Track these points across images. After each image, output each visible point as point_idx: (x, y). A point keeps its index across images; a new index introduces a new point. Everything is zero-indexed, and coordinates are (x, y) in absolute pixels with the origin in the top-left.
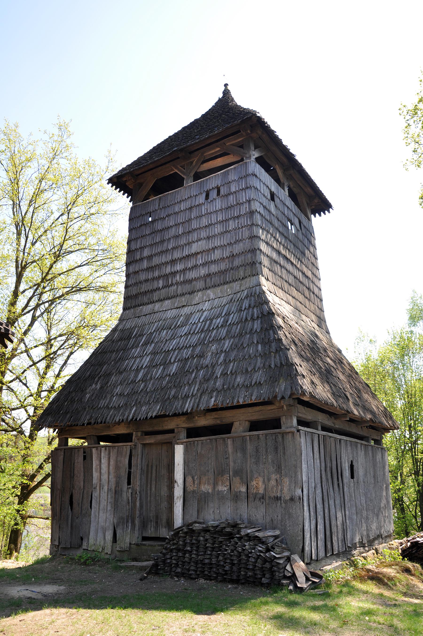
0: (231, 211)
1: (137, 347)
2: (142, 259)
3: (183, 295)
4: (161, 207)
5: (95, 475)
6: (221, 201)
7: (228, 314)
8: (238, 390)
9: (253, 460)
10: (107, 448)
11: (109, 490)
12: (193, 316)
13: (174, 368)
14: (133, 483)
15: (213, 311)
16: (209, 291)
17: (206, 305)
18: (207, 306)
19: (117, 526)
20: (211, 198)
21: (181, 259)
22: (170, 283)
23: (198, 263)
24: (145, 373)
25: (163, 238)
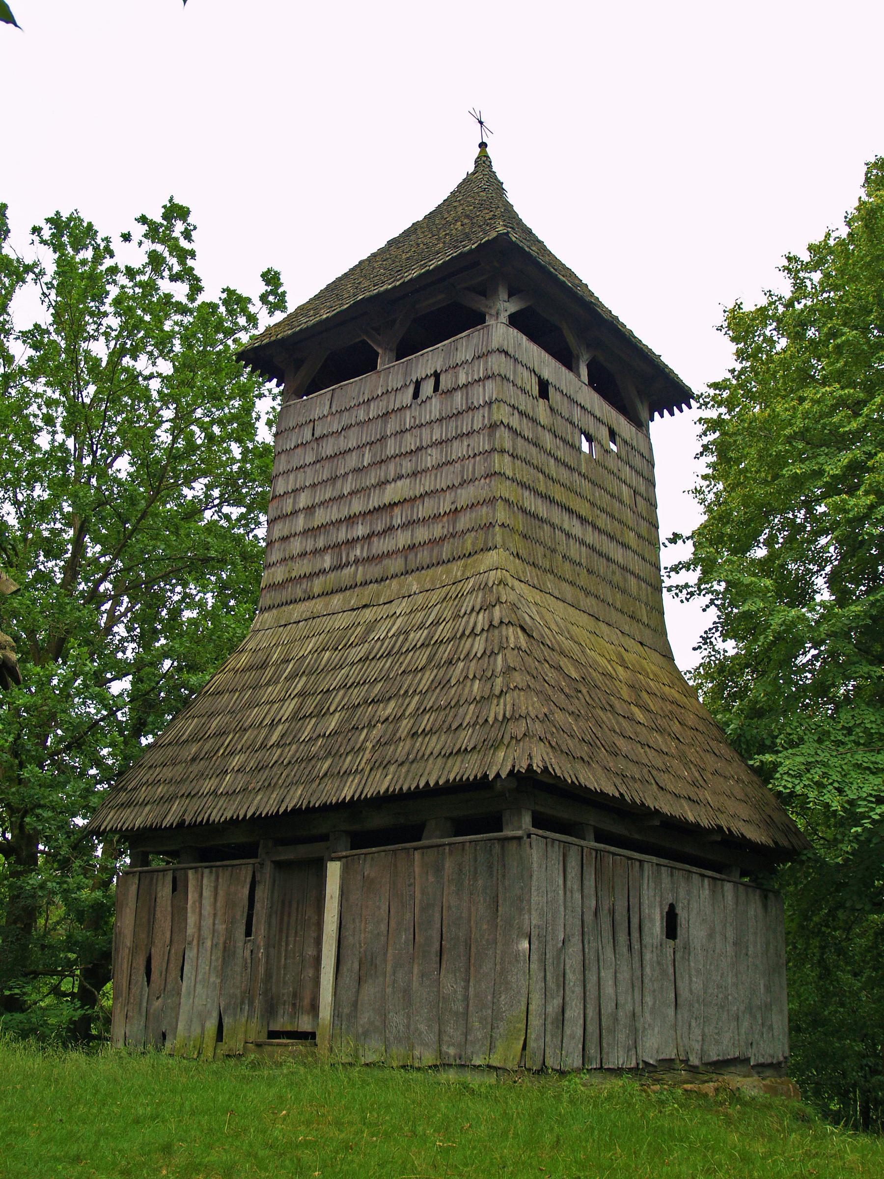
0: (456, 422)
1: (277, 682)
2: (294, 513)
3: (365, 584)
4: (334, 410)
5: (191, 919)
6: (441, 403)
7: (436, 623)
8: (430, 762)
9: (453, 888)
10: (214, 869)
11: (214, 946)
12: (379, 625)
13: (333, 723)
14: (256, 932)
15: (413, 615)
16: (410, 578)
17: (404, 604)
18: (402, 607)
19: (225, 1013)
20: (423, 396)
21: (364, 515)
22: (344, 560)
23: (394, 523)
24: (283, 732)
25: (336, 472)
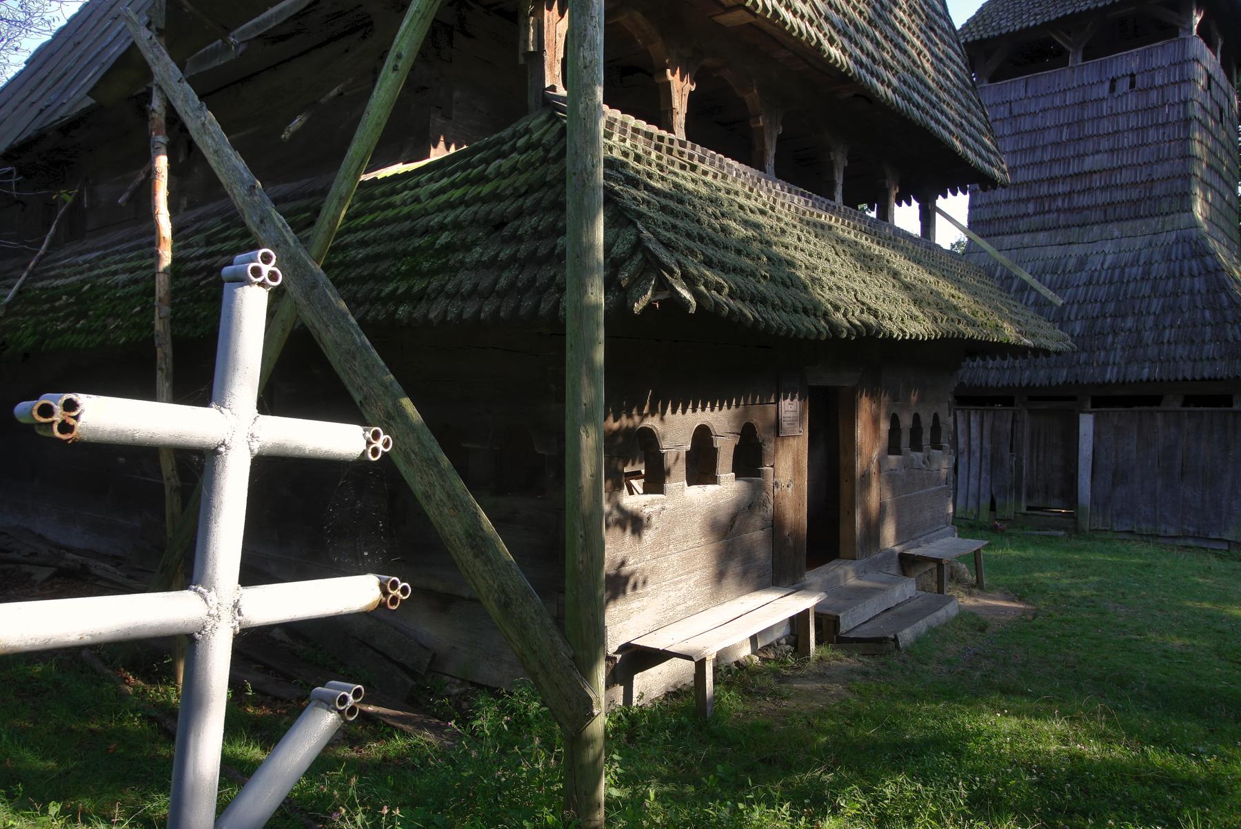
10: (979, 411)
